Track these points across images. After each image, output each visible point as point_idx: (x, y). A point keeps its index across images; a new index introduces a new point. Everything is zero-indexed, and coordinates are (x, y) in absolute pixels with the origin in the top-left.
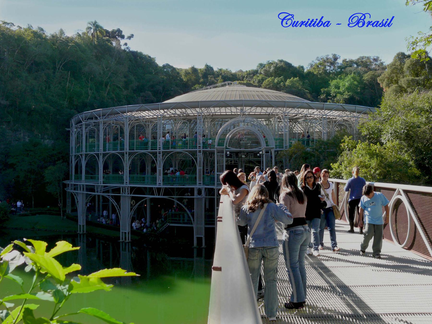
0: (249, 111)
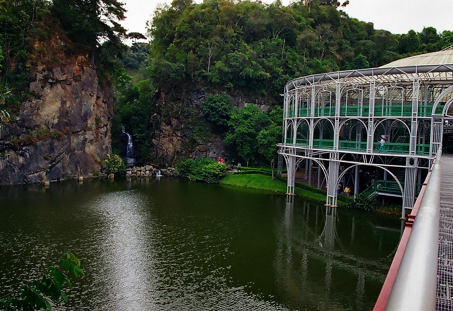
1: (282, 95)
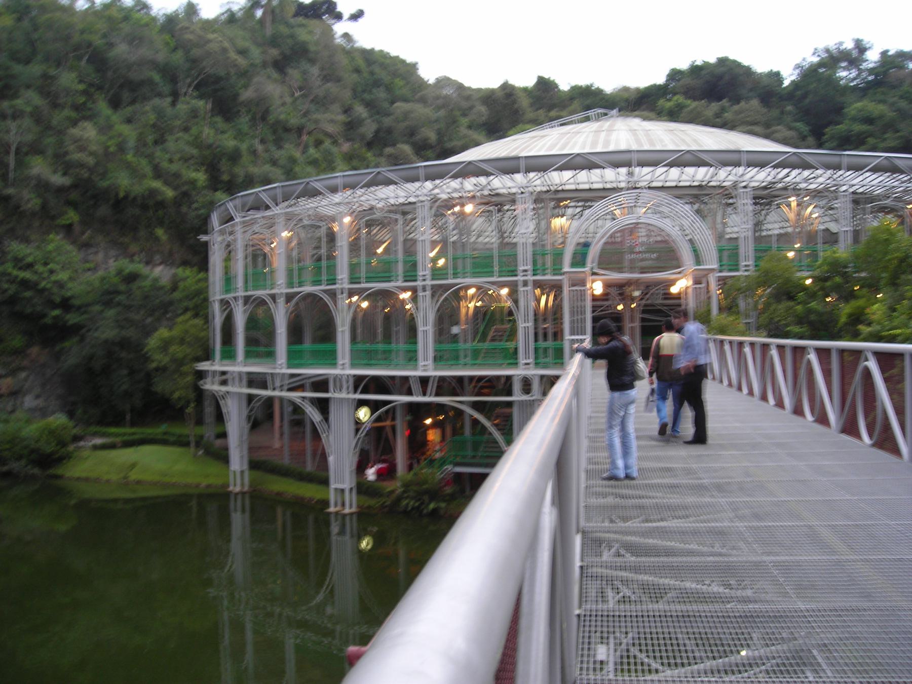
0: (648, 177)
1: (204, 238)
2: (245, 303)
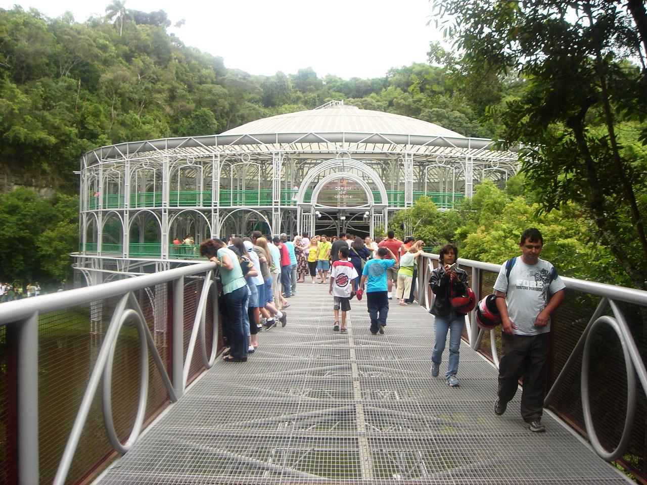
2: (103, 215)
